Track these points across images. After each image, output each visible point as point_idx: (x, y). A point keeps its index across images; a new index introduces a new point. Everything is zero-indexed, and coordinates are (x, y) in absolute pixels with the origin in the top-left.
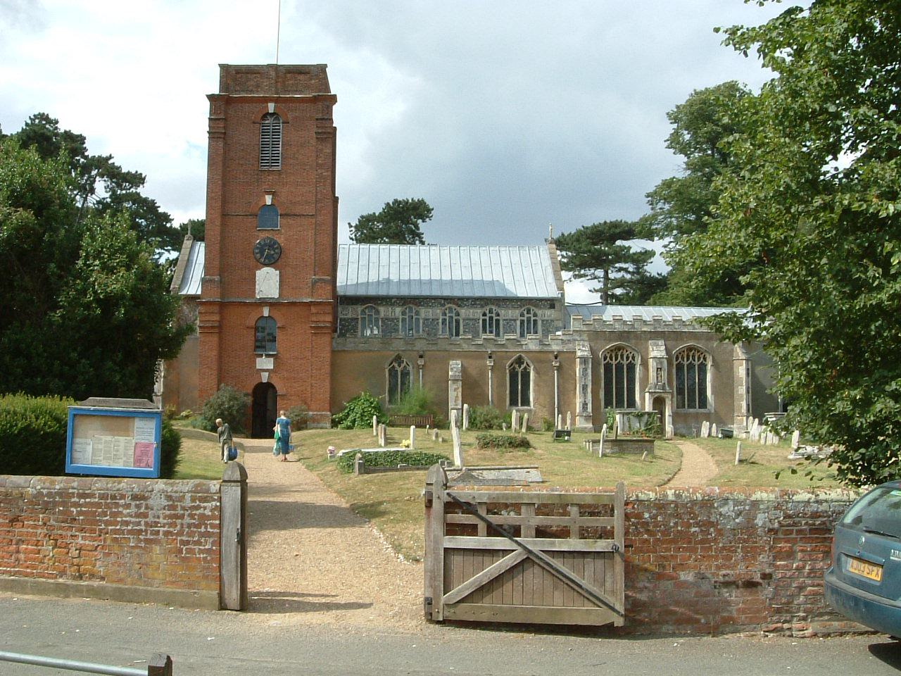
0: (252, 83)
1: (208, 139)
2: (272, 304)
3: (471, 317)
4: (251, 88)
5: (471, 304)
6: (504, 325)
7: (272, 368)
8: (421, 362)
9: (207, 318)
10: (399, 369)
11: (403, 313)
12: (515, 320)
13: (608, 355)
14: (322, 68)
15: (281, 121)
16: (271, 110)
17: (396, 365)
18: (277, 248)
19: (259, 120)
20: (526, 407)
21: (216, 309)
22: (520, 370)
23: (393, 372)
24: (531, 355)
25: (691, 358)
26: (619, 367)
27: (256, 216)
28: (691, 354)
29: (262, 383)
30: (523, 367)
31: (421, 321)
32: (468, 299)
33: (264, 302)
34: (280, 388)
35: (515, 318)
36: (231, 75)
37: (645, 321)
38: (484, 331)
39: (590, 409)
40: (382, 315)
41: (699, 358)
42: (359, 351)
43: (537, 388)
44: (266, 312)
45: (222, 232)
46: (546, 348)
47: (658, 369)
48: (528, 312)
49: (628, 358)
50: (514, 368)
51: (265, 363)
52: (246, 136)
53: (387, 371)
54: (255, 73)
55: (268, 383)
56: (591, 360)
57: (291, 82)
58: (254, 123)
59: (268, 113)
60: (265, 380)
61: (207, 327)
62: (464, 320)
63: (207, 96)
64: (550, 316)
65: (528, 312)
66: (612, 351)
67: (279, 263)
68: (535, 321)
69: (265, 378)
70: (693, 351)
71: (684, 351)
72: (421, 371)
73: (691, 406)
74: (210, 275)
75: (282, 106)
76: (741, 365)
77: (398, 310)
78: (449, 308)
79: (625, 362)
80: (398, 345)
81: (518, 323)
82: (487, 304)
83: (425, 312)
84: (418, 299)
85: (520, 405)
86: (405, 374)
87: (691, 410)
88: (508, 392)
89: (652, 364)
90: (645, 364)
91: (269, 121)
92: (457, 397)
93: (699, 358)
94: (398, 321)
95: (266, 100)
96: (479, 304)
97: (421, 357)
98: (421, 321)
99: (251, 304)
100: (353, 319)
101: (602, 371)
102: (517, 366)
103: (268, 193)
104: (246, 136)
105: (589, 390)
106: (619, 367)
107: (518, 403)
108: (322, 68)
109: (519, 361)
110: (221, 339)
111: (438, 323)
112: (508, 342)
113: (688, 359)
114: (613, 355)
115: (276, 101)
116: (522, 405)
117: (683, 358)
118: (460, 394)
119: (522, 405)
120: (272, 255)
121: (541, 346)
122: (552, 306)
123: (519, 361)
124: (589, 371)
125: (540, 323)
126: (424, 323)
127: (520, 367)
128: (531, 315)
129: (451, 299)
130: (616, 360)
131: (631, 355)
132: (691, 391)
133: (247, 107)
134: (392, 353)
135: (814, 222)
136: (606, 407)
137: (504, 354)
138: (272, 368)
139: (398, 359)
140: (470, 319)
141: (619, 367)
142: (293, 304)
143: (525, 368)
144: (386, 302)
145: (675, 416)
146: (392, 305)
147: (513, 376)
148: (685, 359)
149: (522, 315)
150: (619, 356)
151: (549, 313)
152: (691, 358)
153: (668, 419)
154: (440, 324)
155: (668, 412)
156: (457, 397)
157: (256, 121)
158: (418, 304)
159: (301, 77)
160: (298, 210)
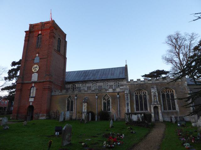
12: (113, 85)
16: (40, 33)
20: (174, 111)
23: (68, 101)
24: (109, 94)
28: (167, 90)
29: (30, 105)
34: (35, 107)
40: (77, 86)
41: (170, 92)
46: (115, 91)
47: (154, 96)
52: (34, 41)
53: (66, 101)
60: (31, 104)
69: (31, 104)
71: (164, 89)
73: (170, 109)
77: (81, 85)
86: (72, 102)
87: (169, 111)
88: (103, 106)
91: (40, 36)
93: (170, 92)
95: (38, 31)
100: (69, 88)
101: (134, 98)
103: (37, 53)
104: (34, 41)
105: (129, 105)
106: (168, 95)
117: (164, 92)
118: (86, 108)
124: (129, 98)
141: (141, 97)
145: (162, 113)
149: (72, 86)
153: (160, 115)
155: (160, 111)
159: (48, 24)
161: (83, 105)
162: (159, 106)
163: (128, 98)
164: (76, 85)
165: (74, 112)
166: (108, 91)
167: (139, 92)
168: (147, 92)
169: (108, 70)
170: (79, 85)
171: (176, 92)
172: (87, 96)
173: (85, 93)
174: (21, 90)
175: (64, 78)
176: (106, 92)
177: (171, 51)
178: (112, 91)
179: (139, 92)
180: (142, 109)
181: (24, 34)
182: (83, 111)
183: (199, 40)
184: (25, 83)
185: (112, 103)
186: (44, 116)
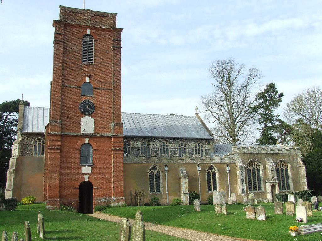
0: (78, 18)
1: (53, 45)
2: (90, 137)
3: (174, 147)
4: (77, 21)
5: (173, 141)
6: (188, 151)
7: (90, 172)
8: (166, 169)
9: (54, 144)
11: (142, 145)
13: (249, 165)
14: (114, 15)
15: (93, 40)
17: (153, 171)
18: (93, 109)
19: (82, 38)
21: (59, 138)
22: (155, 173)
23: (151, 175)
24: (216, 165)
25: (253, 166)
26: (254, 170)
27: (81, 88)
30: (156, 171)
31: (151, 149)
32: (172, 138)
33: (84, 136)
35: (193, 148)
36: (65, 11)
37: (278, 149)
38: (196, 154)
39: (245, 192)
41: (285, 166)
42: (135, 163)
43: (220, 182)
44: (87, 141)
45: (62, 96)
46: (223, 162)
48: (199, 145)
49: (257, 166)
50: (152, 172)
51: (86, 170)
52: (76, 46)
53: (149, 174)
54: (79, 13)
56: (244, 167)
57: (98, 20)
58: (79, 38)
59: (87, 35)
61: (53, 149)
62: (171, 149)
64: (208, 147)
65: (199, 145)
66: (250, 163)
67: (93, 115)
68: (202, 150)
69: (86, 178)
70: (282, 163)
71: (279, 163)
72: (166, 173)
74: (55, 119)
75: (94, 31)
76: (303, 169)
77: (139, 143)
78: (164, 143)
79: (256, 168)
80: (154, 160)
81: (195, 150)
82: (180, 141)
83: (171, 145)
84: (149, 138)
85: (253, 190)
86: (158, 176)
89: (269, 168)
90: (264, 169)
92: (186, 187)
93: (285, 166)
94: (139, 149)
95: (86, 27)
96: (177, 141)
97: (166, 166)
98: (151, 149)
99: (79, 136)
102: (153, 171)
103: (87, 76)
106: (282, 170)
107: (257, 189)
108: (114, 15)
109: (211, 168)
110: (61, 155)
112: (206, 158)
113: (281, 167)
114: (251, 165)
115: (92, 28)
116: (156, 192)
117: (279, 166)
119: (156, 192)
120: (88, 109)
122: (209, 143)
124: (244, 172)
125: (204, 150)
126: (152, 150)
127: (155, 171)
128: (200, 147)
129: (164, 138)
133: (75, 30)
134: (151, 164)
136: (213, 190)
137: (204, 164)
138: (90, 172)
139: (154, 168)
140: (173, 149)
142: (102, 137)
143: (214, 172)
144: (134, 139)
146: (137, 141)
147: (209, 175)
149: (196, 147)
151: (208, 146)
152: (253, 166)
154: (160, 151)
156: (186, 187)
157: (81, 38)
159: (103, 18)
160: (103, 86)
163: (243, 172)
164: (131, 143)
165: (162, 191)
166: (213, 162)
167: (252, 165)
169: (57, 36)
170: (137, 144)
171: (292, 166)
174: (60, 149)
175: (119, 125)
176: (211, 162)
179: (252, 165)
181: (52, 30)
184: (67, 136)
185: (220, 180)
186: (121, 202)
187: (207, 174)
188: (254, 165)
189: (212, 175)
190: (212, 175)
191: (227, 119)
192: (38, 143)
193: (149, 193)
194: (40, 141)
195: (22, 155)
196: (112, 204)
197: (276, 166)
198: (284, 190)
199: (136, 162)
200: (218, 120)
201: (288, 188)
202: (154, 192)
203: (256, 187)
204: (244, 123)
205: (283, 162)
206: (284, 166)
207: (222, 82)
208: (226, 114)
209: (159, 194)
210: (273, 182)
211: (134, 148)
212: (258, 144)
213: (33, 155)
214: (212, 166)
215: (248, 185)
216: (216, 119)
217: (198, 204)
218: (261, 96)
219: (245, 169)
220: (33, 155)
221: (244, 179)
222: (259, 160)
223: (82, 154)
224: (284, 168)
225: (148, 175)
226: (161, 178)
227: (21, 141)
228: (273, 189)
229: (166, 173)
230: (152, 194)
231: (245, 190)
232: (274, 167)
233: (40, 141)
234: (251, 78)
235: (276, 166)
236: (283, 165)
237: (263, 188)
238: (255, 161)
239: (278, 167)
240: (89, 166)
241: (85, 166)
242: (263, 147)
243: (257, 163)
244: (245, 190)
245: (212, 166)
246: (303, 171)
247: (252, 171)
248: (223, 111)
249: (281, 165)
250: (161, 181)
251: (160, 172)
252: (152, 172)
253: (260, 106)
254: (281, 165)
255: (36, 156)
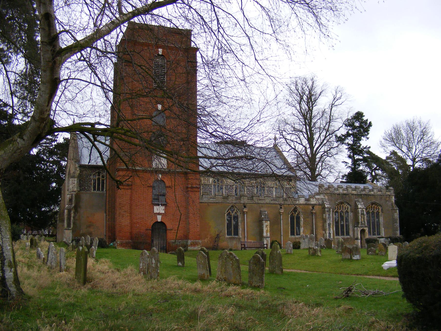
8: (245, 210)
10: (233, 214)
13: (337, 207)
22: (295, 215)
34: (169, 226)
47: (362, 214)
50: (229, 213)
51: (159, 209)
53: (226, 215)
55: (161, 222)
63: (367, 119)
66: (338, 205)
69: (159, 218)
70: (374, 205)
71: (369, 205)
76: (396, 212)
77: (211, 180)
97: (245, 207)
106: (373, 213)
107: (344, 234)
109: (295, 210)
111: (233, 188)
114: (339, 207)
116: (234, 235)
118: (269, 229)
119: (234, 235)
121: (306, 202)
123: (295, 210)
127: (295, 213)
130: (371, 210)
131: (347, 207)
132: (374, 229)
135: (7, 53)
143: (298, 214)
147: (292, 218)
148: (370, 209)
150: (341, 207)
158: (224, 177)
161: (264, 226)
162: (367, 229)
163: (330, 215)
164: (202, 179)
167: (340, 207)
168: (349, 207)
170: (208, 180)
172: (265, 209)
173: (259, 202)
177: (363, 147)
178: (304, 203)
179: (340, 207)
180: (99, 189)
182: (265, 234)
183: (440, 149)
187: (290, 216)
188: (343, 207)
189: (295, 217)
190: (295, 217)
191: (306, 148)
192: (97, 177)
193: (227, 236)
194: (99, 175)
195: (80, 190)
196: (189, 248)
197: (366, 209)
198: (374, 236)
199: (212, 202)
200: (294, 149)
201: (379, 233)
202: (231, 235)
203: (344, 232)
204: (325, 154)
205: (374, 204)
206: (375, 209)
207: (301, 101)
208: (305, 142)
209: (237, 238)
210: (363, 227)
211: (205, 185)
212: (344, 180)
213: (92, 191)
214: (296, 208)
215: (334, 229)
216: (291, 147)
217: (290, 247)
218: (349, 124)
219: (333, 212)
220: (92, 191)
221: (331, 222)
222: (348, 202)
223: (318, 206)
224: (376, 211)
225: (225, 216)
226: (240, 219)
227: (79, 174)
228: (362, 235)
229: (245, 215)
230: (230, 238)
231: (332, 235)
232: (364, 210)
233: (99, 175)
234: (337, 97)
235: (367, 208)
236: (374, 208)
237: (351, 233)
238: (343, 203)
239: (368, 209)
240: (162, 205)
241: (158, 205)
242: (353, 185)
243: (345, 205)
244: (332, 235)
245: (296, 208)
246: (98, 241)
247: (376, 214)
248: (302, 137)
249: (372, 207)
250: (240, 224)
251: (239, 214)
252: (229, 213)
253: (348, 135)
254: (372, 207)
255: (95, 192)
